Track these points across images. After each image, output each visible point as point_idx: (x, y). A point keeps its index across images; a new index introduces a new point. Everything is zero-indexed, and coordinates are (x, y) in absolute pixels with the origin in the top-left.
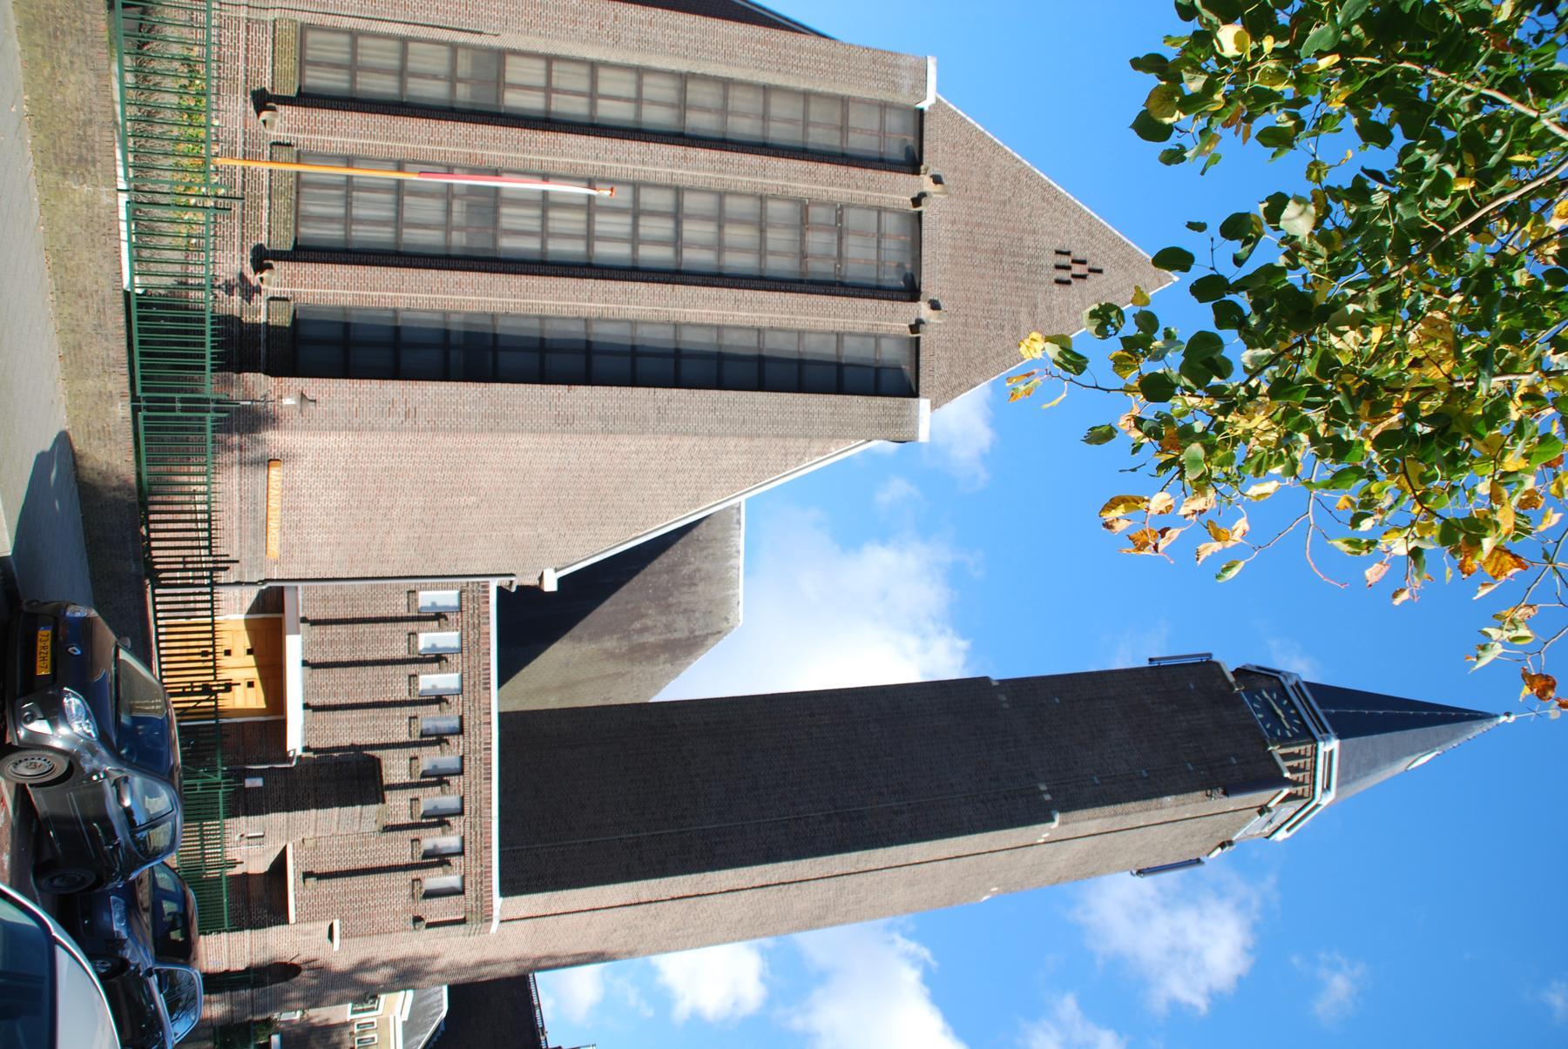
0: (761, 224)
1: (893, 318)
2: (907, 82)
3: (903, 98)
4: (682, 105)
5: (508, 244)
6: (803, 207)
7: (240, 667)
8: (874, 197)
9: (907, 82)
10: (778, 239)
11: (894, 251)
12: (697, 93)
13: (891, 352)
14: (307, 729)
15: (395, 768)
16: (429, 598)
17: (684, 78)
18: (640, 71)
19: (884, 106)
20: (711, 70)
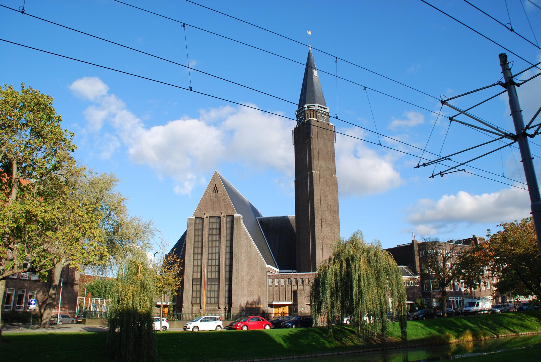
0: (212, 241)
1: (224, 220)
2: (191, 221)
3: (193, 222)
4: (198, 254)
5: (217, 277)
6: (209, 235)
7: (281, 310)
8: (207, 225)
9: (191, 221)
10: (215, 226)
11: (215, 220)
12: (196, 252)
13: (229, 219)
14: (288, 301)
15: (295, 288)
16: (270, 284)
17: (194, 254)
18: (194, 260)
19: (195, 223)
20: (192, 250)
